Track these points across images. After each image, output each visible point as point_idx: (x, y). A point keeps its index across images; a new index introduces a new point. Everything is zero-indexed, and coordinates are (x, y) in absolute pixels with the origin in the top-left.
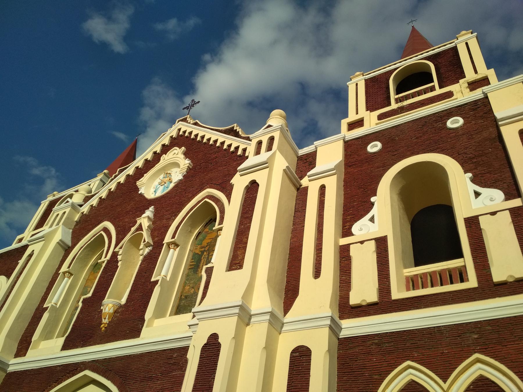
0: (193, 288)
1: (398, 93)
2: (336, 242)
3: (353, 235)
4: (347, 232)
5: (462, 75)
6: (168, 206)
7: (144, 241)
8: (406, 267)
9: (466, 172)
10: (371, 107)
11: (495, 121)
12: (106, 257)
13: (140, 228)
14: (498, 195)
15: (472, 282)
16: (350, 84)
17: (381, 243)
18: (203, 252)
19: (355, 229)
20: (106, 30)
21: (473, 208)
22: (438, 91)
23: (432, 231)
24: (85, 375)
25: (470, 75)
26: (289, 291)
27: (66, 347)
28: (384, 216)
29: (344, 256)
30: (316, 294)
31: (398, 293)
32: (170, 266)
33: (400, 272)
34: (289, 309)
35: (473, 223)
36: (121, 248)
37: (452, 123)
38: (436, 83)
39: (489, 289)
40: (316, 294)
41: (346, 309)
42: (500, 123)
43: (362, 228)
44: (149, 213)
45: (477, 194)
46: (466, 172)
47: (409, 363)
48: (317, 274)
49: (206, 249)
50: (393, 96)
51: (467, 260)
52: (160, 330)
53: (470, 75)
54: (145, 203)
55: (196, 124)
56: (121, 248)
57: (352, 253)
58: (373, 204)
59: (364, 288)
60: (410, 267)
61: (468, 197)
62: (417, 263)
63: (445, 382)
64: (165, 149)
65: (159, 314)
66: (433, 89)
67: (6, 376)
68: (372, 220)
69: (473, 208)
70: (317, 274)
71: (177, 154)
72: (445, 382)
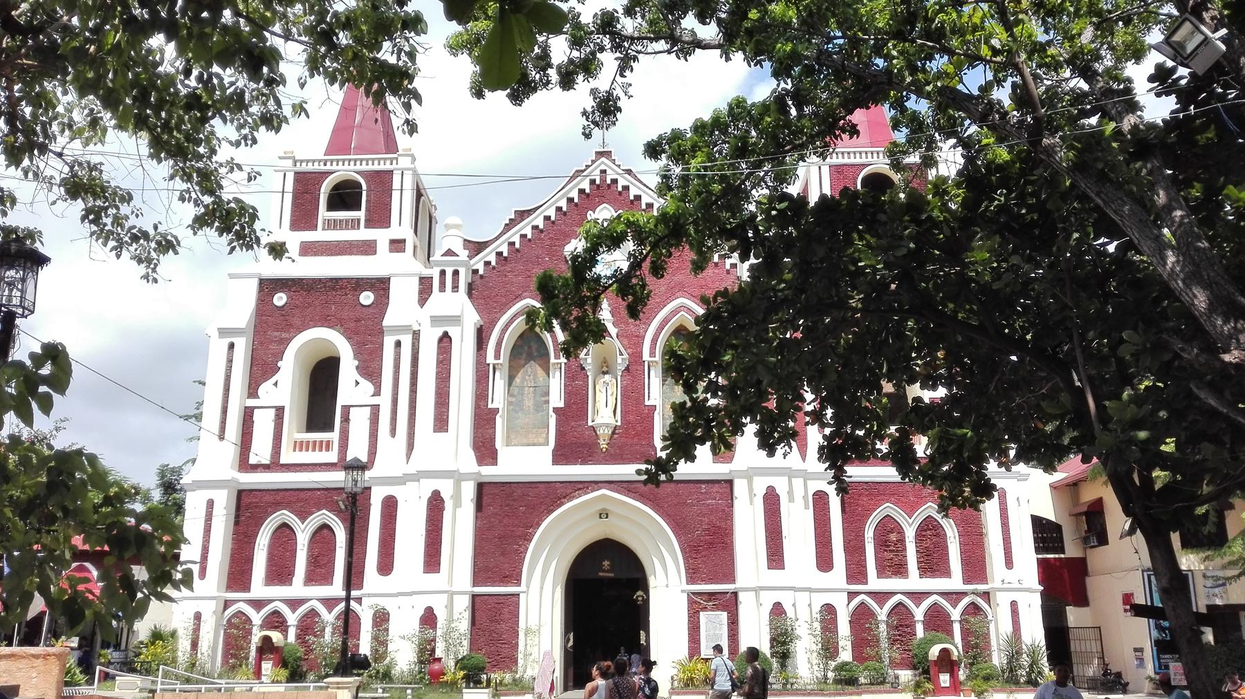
4: (253, 392)
7: (621, 354)
15: (332, 456)
17: (280, 411)
20: (606, 563)
21: (725, 614)
22: (363, 234)
28: (286, 387)
31: (287, 457)
33: (293, 431)
35: (346, 409)
38: (361, 214)
41: (244, 464)
45: (357, 383)
48: (393, 432)
51: (334, 436)
61: (351, 388)
66: (354, 224)
69: (725, 614)
70: (393, 432)
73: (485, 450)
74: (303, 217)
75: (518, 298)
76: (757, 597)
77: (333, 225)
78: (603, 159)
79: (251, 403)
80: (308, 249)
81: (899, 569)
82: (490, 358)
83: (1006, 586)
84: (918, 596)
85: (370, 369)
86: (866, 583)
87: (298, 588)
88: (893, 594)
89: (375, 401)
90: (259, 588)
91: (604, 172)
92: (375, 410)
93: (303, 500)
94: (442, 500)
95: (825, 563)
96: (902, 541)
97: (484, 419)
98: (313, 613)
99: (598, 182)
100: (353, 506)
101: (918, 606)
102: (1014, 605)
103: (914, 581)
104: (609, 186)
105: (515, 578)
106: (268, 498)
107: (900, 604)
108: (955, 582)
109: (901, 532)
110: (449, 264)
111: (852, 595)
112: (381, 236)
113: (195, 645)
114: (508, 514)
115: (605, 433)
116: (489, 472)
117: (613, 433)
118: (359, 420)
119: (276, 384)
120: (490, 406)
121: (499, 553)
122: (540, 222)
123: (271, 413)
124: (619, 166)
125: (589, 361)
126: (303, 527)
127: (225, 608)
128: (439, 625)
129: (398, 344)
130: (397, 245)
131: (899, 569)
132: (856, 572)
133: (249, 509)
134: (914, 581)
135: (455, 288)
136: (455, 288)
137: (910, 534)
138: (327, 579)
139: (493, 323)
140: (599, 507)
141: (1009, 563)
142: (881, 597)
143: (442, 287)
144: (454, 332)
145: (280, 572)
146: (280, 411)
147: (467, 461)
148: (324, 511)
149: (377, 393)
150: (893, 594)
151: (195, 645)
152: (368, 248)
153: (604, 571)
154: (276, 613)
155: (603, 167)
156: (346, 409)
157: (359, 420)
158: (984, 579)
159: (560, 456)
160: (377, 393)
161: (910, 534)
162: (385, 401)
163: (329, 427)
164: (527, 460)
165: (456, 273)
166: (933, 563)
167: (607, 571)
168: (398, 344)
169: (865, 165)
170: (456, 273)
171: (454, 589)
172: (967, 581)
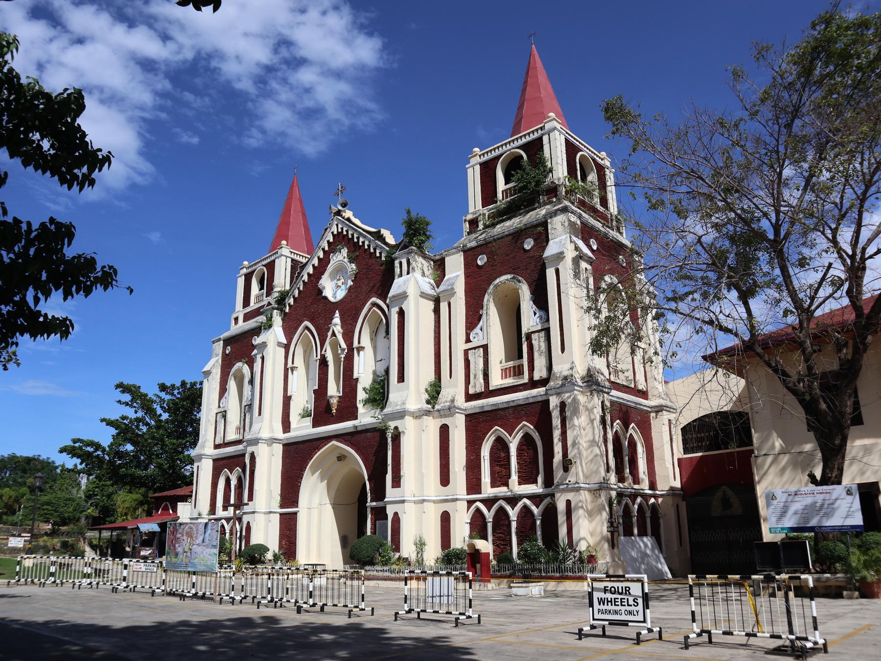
6: (350, 309)
27: (314, 426)
64: (333, 248)
80: (247, 317)
86: (480, 493)
90: (488, 490)
92: (547, 331)
98: (501, 510)
99: (335, 233)
103: (516, 487)
111: (470, 503)
140: (336, 454)
154: (525, 507)
156: (529, 336)
169: (497, 158)
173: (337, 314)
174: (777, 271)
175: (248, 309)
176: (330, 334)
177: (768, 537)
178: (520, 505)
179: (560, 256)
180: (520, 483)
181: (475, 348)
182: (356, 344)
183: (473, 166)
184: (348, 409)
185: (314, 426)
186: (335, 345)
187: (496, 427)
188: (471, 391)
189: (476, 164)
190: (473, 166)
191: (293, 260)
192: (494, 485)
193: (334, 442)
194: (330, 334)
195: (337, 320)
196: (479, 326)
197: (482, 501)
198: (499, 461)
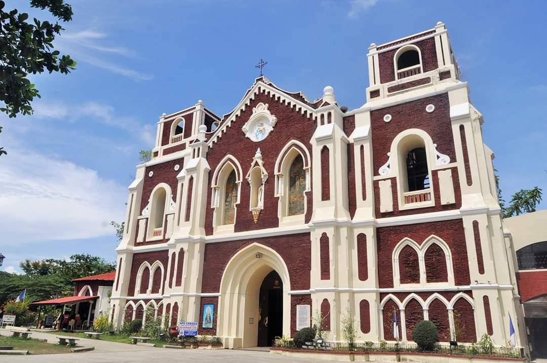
0: (295, 197)
1: (399, 69)
2: (372, 178)
3: (380, 175)
4: (376, 173)
5: (436, 67)
6: (270, 147)
7: (263, 173)
8: (405, 192)
9: (434, 143)
10: (383, 80)
11: (450, 118)
12: (239, 180)
13: (257, 164)
14: (447, 158)
15: (431, 203)
16: (369, 56)
18: (295, 176)
19: (380, 171)
22: (422, 75)
23: (416, 170)
24: (255, 245)
25: (441, 68)
26: (352, 207)
27: (235, 231)
28: (394, 167)
29: (376, 185)
30: (365, 212)
32: (281, 189)
34: (354, 214)
35: (435, 173)
36: (249, 176)
37: (429, 108)
38: (421, 65)
39: (439, 207)
40: (365, 212)
41: (378, 214)
42: (451, 119)
43: (384, 171)
44: (258, 154)
45: (438, 157)
46: (434, 143)
47: (406, 238)
48: (364, 198)
49: (297, 174)
50: (396, 71)
51: (162, 229)
52: (289, 224)
53: (441, 68)
54: (253, 146)
55: (270, 85)
56: (249, 176)
57: (380, 186)
58: (389, 157)
59: (386, 205)
60: (407, 192)
61: (435, 160)
62: (410, 190)
63: (420, 245)
64: (254, 103)
65: (284, 215)
66: (417, 71)
67: (308, 328)
68: (389, 167)
70: (364, 198)
71: (261, 109)
72: (420, 245)
73: (209, 230)
74: (387, 76)
75: (289, 139)
76: (499, 293)
77: (401, 76)
78: (259, 82)
79: (376, 178)
80: (166, 152)
81: (415, 279)
82: (213, 185)
83: (479, 285)
84: (425, 294)
85: (446, 147)
86: (393, 287)
87: (148, 295)
88: (409, 293)
89: (453, 165)
90: (137, 295)
91: (260, 88)
92: (455, 171)
93: (418, 231)
94: (328, 238)
95: (363, 275)
96: (416, 260)
97: (209, 212)
98: (141, 305)
99: (257, 93)
100: (453, 230)
101: (425, 300)
102: (486, 299)
103: (423, 285)
104: (262, 93)
105: (217, 289)
106: (142, 257)
107: (390, 300)
108: (450, 285)
109: (416, 255)
110: (196, 146)
112: (433, 74)
113: (112, 318)
114: (216, 256)
115: (255, 214)
116: (209, 238)
117: (260, 213)
118: (445, 180)
119: (147, 209)
120: (212, 207)
121: (211, 279)
122: (234, 119)
123: (145, 220)
124: (266, 83)
125: (250, 179)
126: (420, 247)
127: (127, 302)
128: (179, 310)
129: (362, 147)
130: (444, 75)
131: (415, 279)
132: (385, 279)
133: (386, 237)
134: (423, 285)
135: (329, 122)
136: (329, 122)
137: (421, 255)
138: (157, 292)
139: (214, 169)
140: (256, 252)
141: (482, 270)
142: (401, 295)
143: (323, 123)
144: (195, 176)
145: (143, 290)
146: (393, 180)
147: (200, 234)
148: (432, 235)
149: (453, 160)
150: (409, 293)
151: (112, 318)
152: (426, 81)
153: (275, 286)
154: (390, 300)
155: (259, 86)
156: (435, 173)
157: (445, 180)
158: (468, 283)
159: (238, 229)
160: (453, 160)
161: (421, 255)
162: (460, 164)
163: (421, 186)
164: (225, 232)
165: (329, 114)
166: (436, 273)
167: (278, 286)
168: (362, 147)
170: (329, 114)
171: (354, 289)
172: (457, 284)
173: (259, 150)
174: (292, 197)
175: (166, 147)
176: (253, 164)
177: (297, 330)
178: (138, 303)
179: (183, 178)
180: (428, 281)
181: (384, 180)
182: (276, 173)
183: (161, 123)
184: (269, 217)
185: (235, 231)
186: (258, 173)
187: (158, 261)
188: (138, 242)
189: (198, 110)
190: (161, 123)
191: (206, 114)
192: (403, 281)
193: (255, 244)
194: (253, 164)
195: (258, 154)
196: (387, 164)
197: (394, 293)
198: (409, 264)
